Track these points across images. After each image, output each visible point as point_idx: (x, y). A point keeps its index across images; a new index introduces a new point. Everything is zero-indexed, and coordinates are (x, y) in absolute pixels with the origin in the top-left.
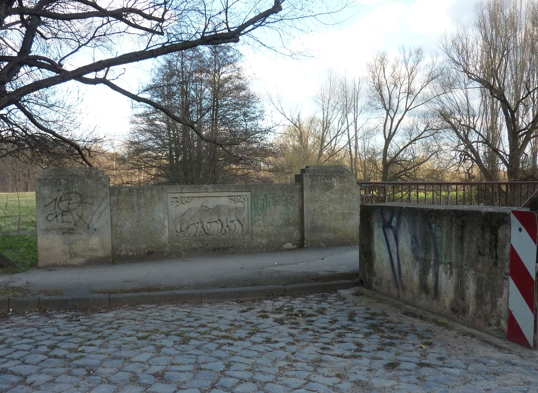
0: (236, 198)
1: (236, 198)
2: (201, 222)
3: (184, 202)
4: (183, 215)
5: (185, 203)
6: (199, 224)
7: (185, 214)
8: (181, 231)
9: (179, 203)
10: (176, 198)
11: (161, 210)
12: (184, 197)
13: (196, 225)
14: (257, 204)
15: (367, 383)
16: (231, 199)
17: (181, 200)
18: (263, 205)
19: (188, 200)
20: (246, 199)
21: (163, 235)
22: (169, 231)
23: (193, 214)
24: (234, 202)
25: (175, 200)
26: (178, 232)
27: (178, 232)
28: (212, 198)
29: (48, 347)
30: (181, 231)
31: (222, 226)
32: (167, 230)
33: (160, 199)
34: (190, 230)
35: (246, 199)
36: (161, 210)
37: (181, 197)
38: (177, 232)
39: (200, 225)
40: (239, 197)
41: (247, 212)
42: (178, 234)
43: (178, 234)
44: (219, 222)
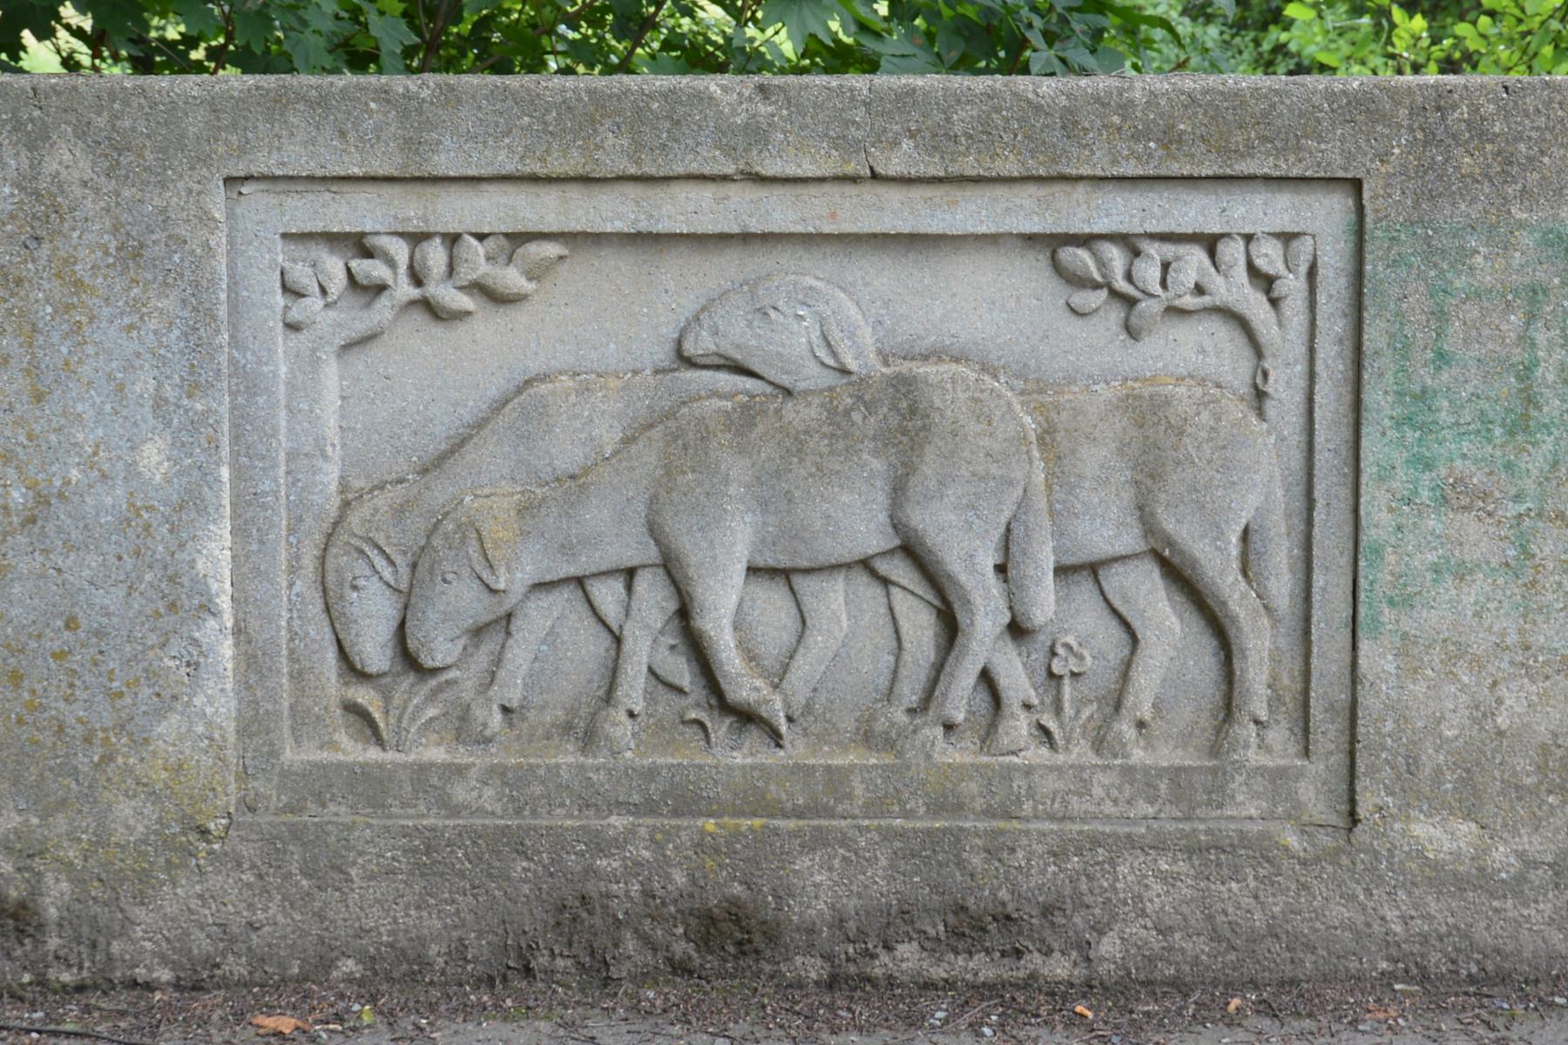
0: (1149, 273)
1: (1149, 273)
2: (671, 567)
3: (450, 296)
4: (440, 460)
5: (462, 315)
6: (643, 583)
7: (459, 444)
8: (408, 659)
9: (383, 309)
10: (360, 245)
11: (143, 384)
12: (453, 240)
13: (608, 595)
14: (1442, 358)
15: (1272, 659)
16: (1076, 280)
17: (417, 280)
18: (1526, 372)
19: (512, 278)
20: (1292, 285)
21: (167, 703)
22: (252, 661)
23: (566, 453)
24: (1115, 314)
25: (334, 266)
26: (362, 676)
27: (362, 676)
28: (813, 271)
29: (670, 960)
30: (408, 659)
31: (950, 626)
32: (227, 649)
33: (132, 254)
34: (520, 655)
35: (1292, 285)
36: (143, 384)
37: (417, 239)
38: (352, 669)
39: (653, 598)
40: (1196, 256)
41: (1296, 438)
42: (364, 696)
43: (364, 696)
44: (900, 570)
